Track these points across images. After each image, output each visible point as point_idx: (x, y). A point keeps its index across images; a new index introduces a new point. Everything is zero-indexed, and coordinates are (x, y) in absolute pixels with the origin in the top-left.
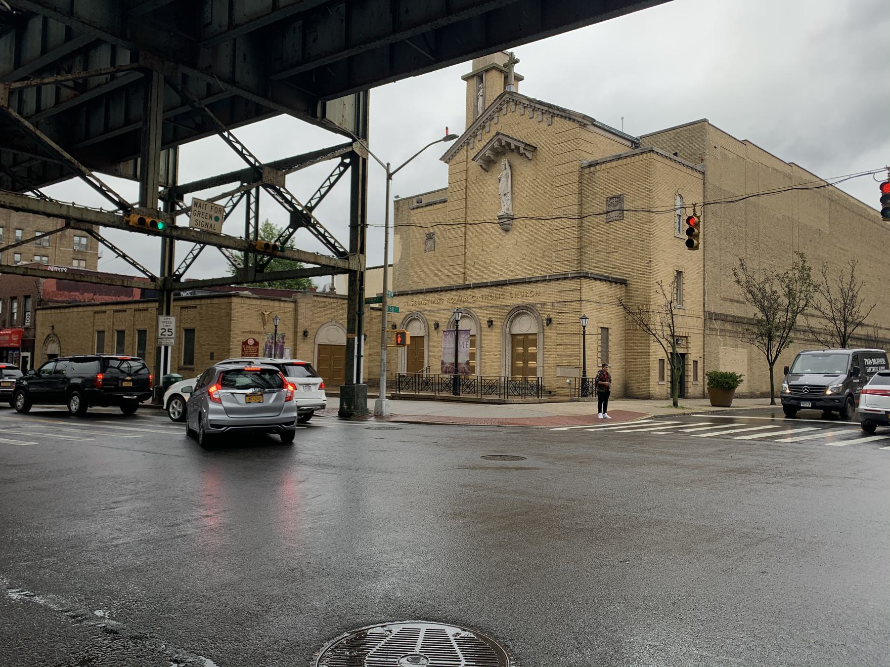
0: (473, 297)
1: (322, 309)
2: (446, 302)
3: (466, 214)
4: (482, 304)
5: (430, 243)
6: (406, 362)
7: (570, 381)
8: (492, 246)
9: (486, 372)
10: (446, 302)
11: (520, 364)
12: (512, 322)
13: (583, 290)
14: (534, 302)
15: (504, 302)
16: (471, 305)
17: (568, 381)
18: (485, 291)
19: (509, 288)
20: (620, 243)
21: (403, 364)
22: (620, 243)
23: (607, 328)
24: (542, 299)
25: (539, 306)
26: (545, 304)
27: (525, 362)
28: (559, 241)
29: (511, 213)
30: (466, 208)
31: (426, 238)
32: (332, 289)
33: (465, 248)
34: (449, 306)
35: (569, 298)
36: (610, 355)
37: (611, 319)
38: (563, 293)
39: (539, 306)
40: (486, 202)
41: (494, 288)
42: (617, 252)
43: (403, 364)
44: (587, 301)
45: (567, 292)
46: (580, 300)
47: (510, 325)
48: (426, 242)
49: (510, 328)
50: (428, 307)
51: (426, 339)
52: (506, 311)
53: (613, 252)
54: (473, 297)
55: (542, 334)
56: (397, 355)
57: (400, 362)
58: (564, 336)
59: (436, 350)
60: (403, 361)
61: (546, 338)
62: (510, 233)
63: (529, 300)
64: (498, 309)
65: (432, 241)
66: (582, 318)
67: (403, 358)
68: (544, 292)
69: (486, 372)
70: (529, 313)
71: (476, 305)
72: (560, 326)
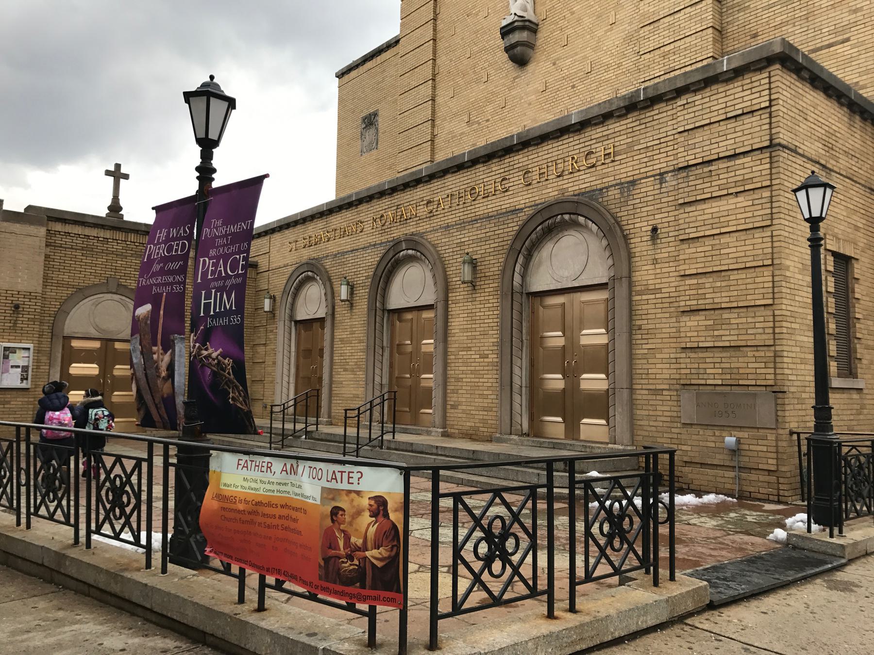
0: (429, 202)
1: (79, 253)
2: (368, 228)
3: (435, 52)
4: (451, 219)
5: (370, 134)
6: (292, 380)
7: (738, 441)
8: (490, 108)
9: (460, 404)
10: (368, 228)
11: (555, 381)
12: (529, 257)
13: (780, 108)
14: (598, 184)
15: (506, 203)
16: (423, 227)
17: (730, 440)
18: (455, 182)
19: (520, 159)
20: (856, 11)
21: (285, 384)
22: (856, 11)
23: (850, 258)
24: (625, 170)
25: (614, 193)
26: (633, 183)
27: (571, 375)
28: (657, 52)
29: (529, 15)
30: (434, 40)
31: (364, 126)
32: (115, 208)
33: (433, 126)
34: (377, 239)
35: (724, 148)
36: (860, 351)
37: (857, 228)
38: (699, 136)
39: (614, 193)
40: (477, 14)
41: (481, 168)
42: (848, 40)
43: (285, 384)
44: (794, 151)
45: (715, 128)
46: (773, 146)
47: (526, 266)
48: (362, 135)
49: (523, 276)
50: (333, 247)
51: (328, 324)
52: (513, 227)
53: (830, 46)
54: (429, 202)
55: (625, 282)
56: (274, 363)
57: (279, 381)
58: (707, 281)
59: (347, 350)
60: (286, 379)
61: (640, 293)
62: (531, 67)
63: (584, 181)
64: (490, 226)
65: (372, 131)
66: (805, 187)
67: (286, 372)
68: (630, 146)
69: (460, 404)
70: (581, 219)
71: (436, 222)
72: (689, 250)
